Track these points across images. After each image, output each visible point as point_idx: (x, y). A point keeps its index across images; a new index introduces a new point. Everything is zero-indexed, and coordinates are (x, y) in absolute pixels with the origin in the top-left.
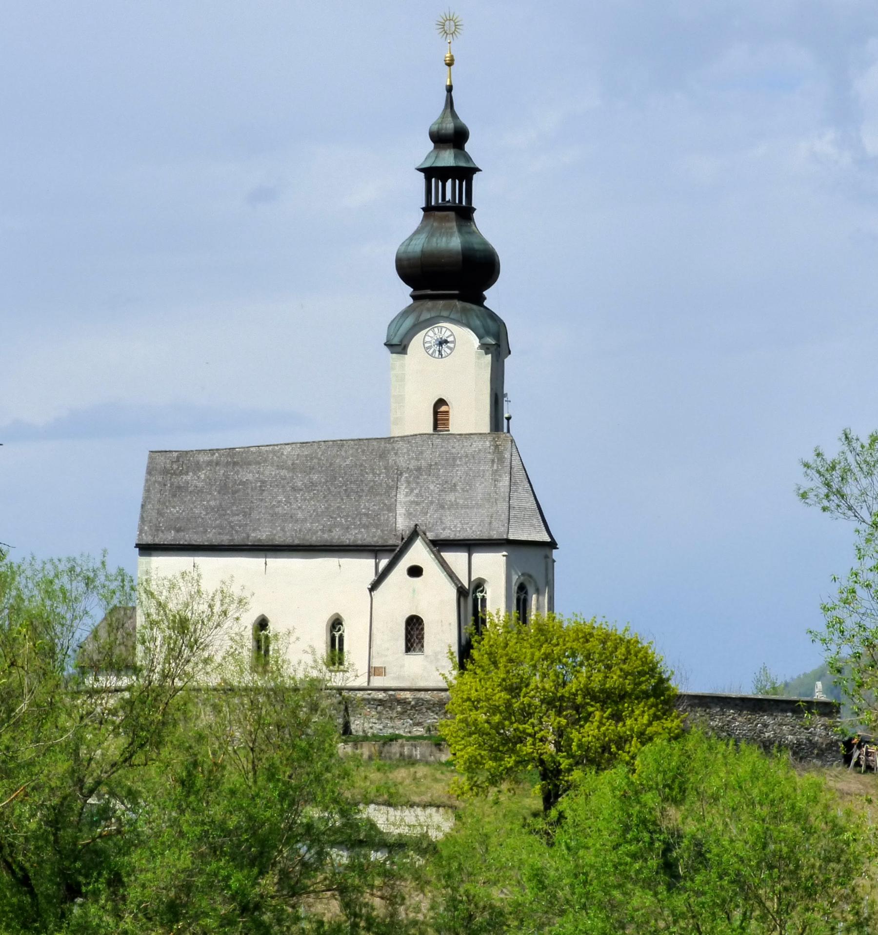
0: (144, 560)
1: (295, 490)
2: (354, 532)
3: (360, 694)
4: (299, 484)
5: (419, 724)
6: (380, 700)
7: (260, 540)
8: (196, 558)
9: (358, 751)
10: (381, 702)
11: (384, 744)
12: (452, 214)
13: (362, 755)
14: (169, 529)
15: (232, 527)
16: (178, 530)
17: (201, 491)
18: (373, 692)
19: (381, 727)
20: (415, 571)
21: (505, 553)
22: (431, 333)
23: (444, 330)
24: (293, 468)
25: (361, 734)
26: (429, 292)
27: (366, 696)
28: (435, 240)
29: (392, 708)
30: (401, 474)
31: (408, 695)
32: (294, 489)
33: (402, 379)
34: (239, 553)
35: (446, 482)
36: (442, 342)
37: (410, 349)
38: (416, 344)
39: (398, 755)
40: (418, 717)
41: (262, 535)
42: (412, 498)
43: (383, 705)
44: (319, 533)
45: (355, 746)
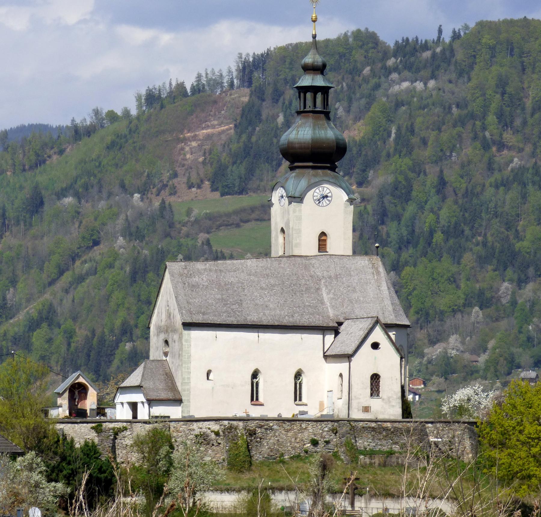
0: (186, 332)
1: (263, 289)
2: (307, 317)
3: (361, 424)
4: (264, 286)
5: (396, 443)
6: (373, 428)
7: (253, 321)
8: (261, 335)
9: (373, 461)
10: (373, 429)
11: (388, 456)
12: (322, 116)
13: (375, 463)
14: (199, 313)
15: (234, 312)
16: (204, 314)
17: (207, 287)
18: (369, 423)
19: (374, 445)
20: (375, 346)
21: (394, 333)
22: (317, 191)
23: (325, 189)
24: (256, 274)
25: (362, 449)
26: (311, 164)
27: (365, 425)
28: (317, 132)
29: (380, 433)
30: (320, 280)
31: (389, 425)
32: (262, 288)
33: (299, 218)
34: (295, 330)
35: (349, 286)
36: (325, 197)
37: (306, 200)
38: (309, 197)
39: (396, 463)
40: (395, 438)
41: (253, 318)
42: (331, 296)
43: (375, 431)
44: (287, 318)
45: (371, 458)
